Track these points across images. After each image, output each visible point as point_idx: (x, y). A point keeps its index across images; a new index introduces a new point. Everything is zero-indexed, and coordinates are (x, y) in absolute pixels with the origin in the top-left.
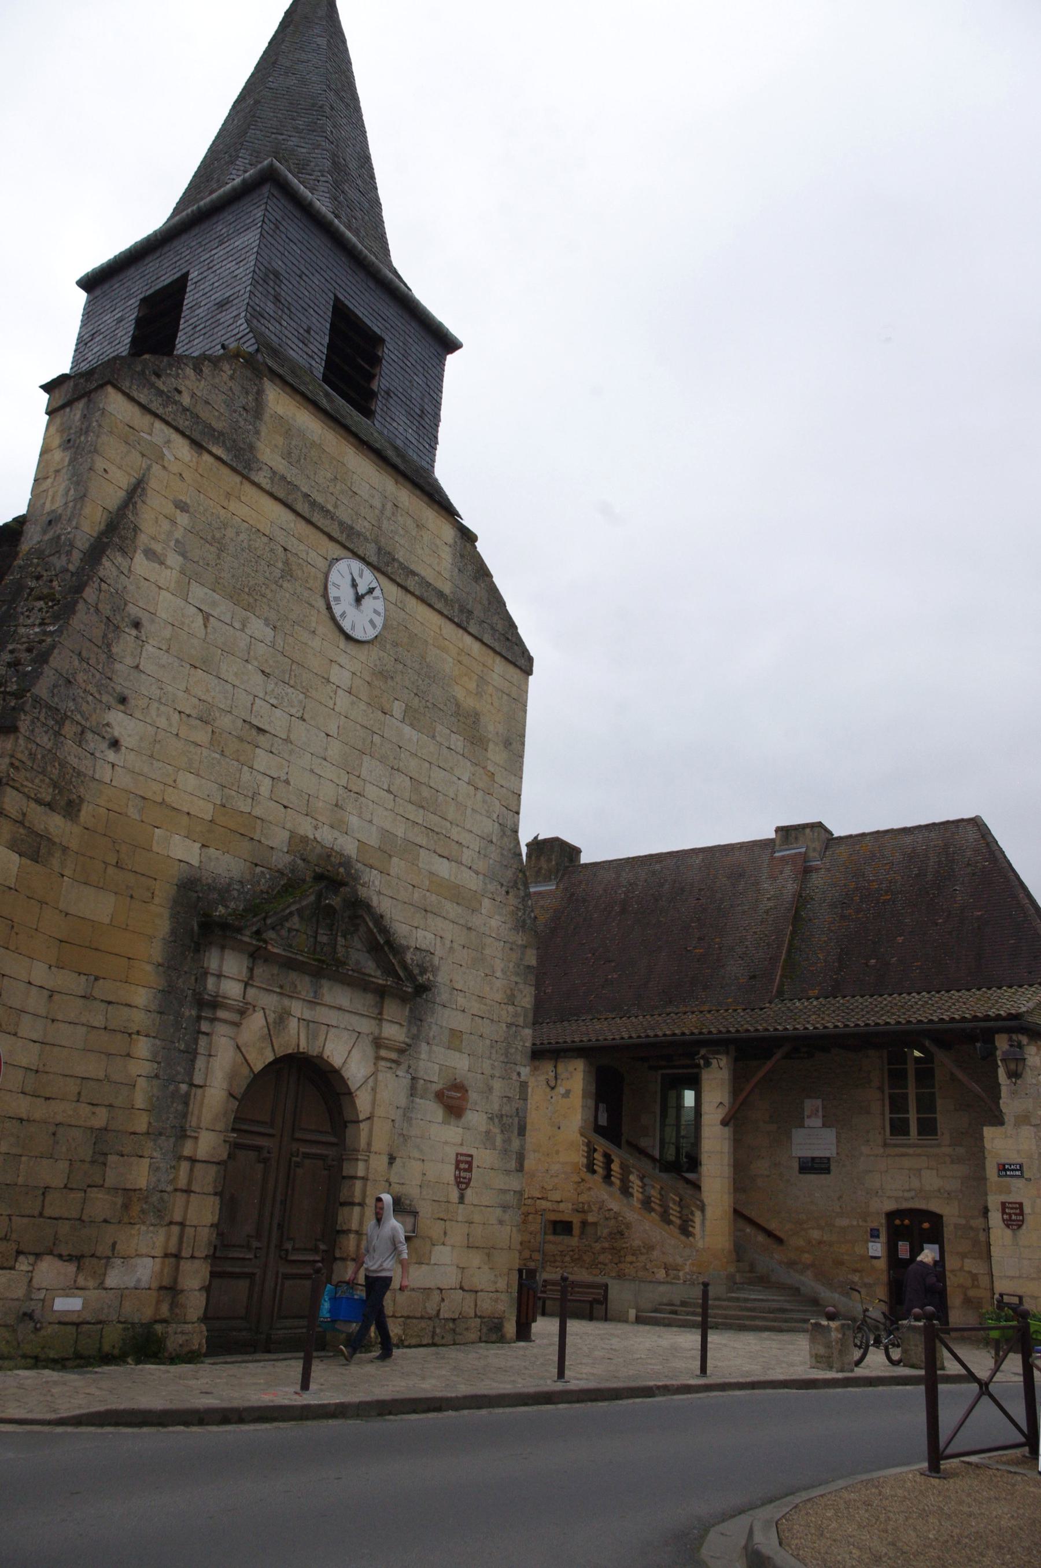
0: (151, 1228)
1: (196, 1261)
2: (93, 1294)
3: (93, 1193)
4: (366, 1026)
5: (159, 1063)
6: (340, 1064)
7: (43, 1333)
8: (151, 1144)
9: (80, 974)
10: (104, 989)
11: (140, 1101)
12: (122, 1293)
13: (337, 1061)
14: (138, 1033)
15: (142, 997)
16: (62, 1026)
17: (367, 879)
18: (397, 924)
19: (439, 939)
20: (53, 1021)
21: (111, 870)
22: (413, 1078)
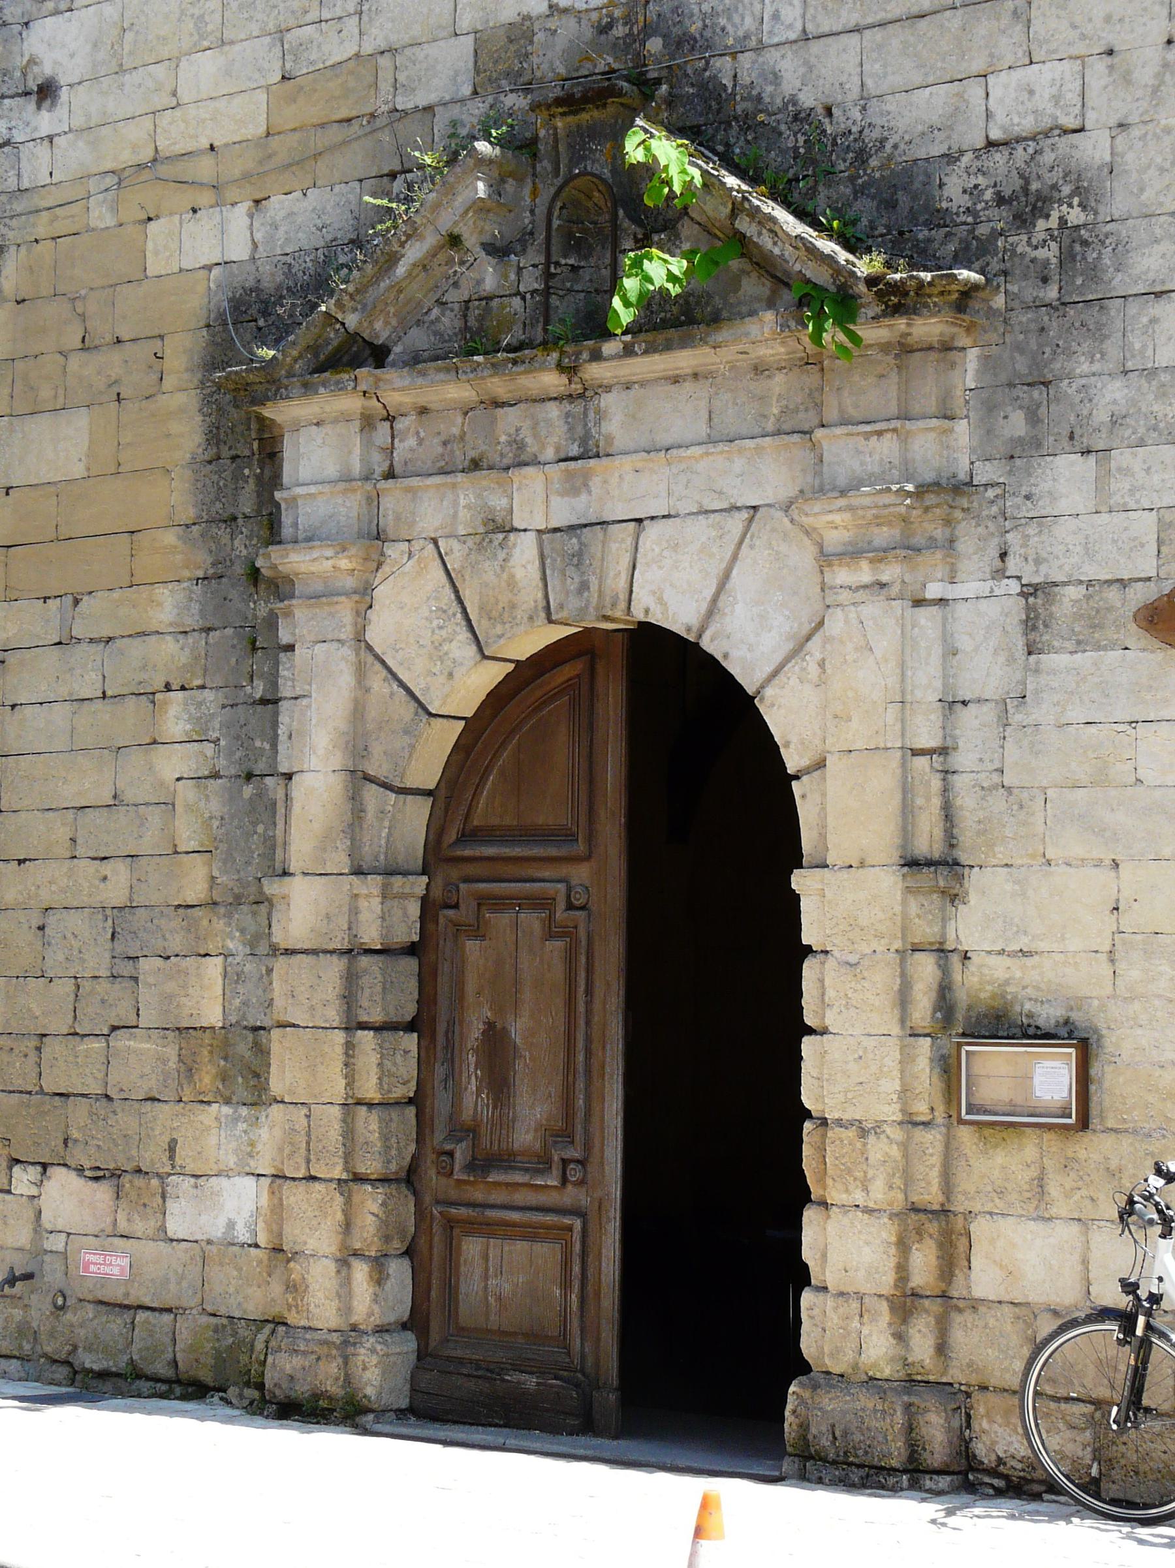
0: (244, 1111)
1: (317, 1186)
2: (150, 1249)
3: (121, 1041)
4: (769, 475)
5: (216, 742)
6: (695, 622)
7: (69, 1316)
8: (220, 924)
9: (45, 599)
10: (96, 615)
11: (188, 835)
12: (205, 1252)
13: (678, 615)
14: (168, 688)
15: (168, 606)
16: (28, 710)
17: (749, 23)
18: (891, 105)
19: (1099, 66)
20: (13, 706)
21: (75, 362)
22: (1030, 591)
